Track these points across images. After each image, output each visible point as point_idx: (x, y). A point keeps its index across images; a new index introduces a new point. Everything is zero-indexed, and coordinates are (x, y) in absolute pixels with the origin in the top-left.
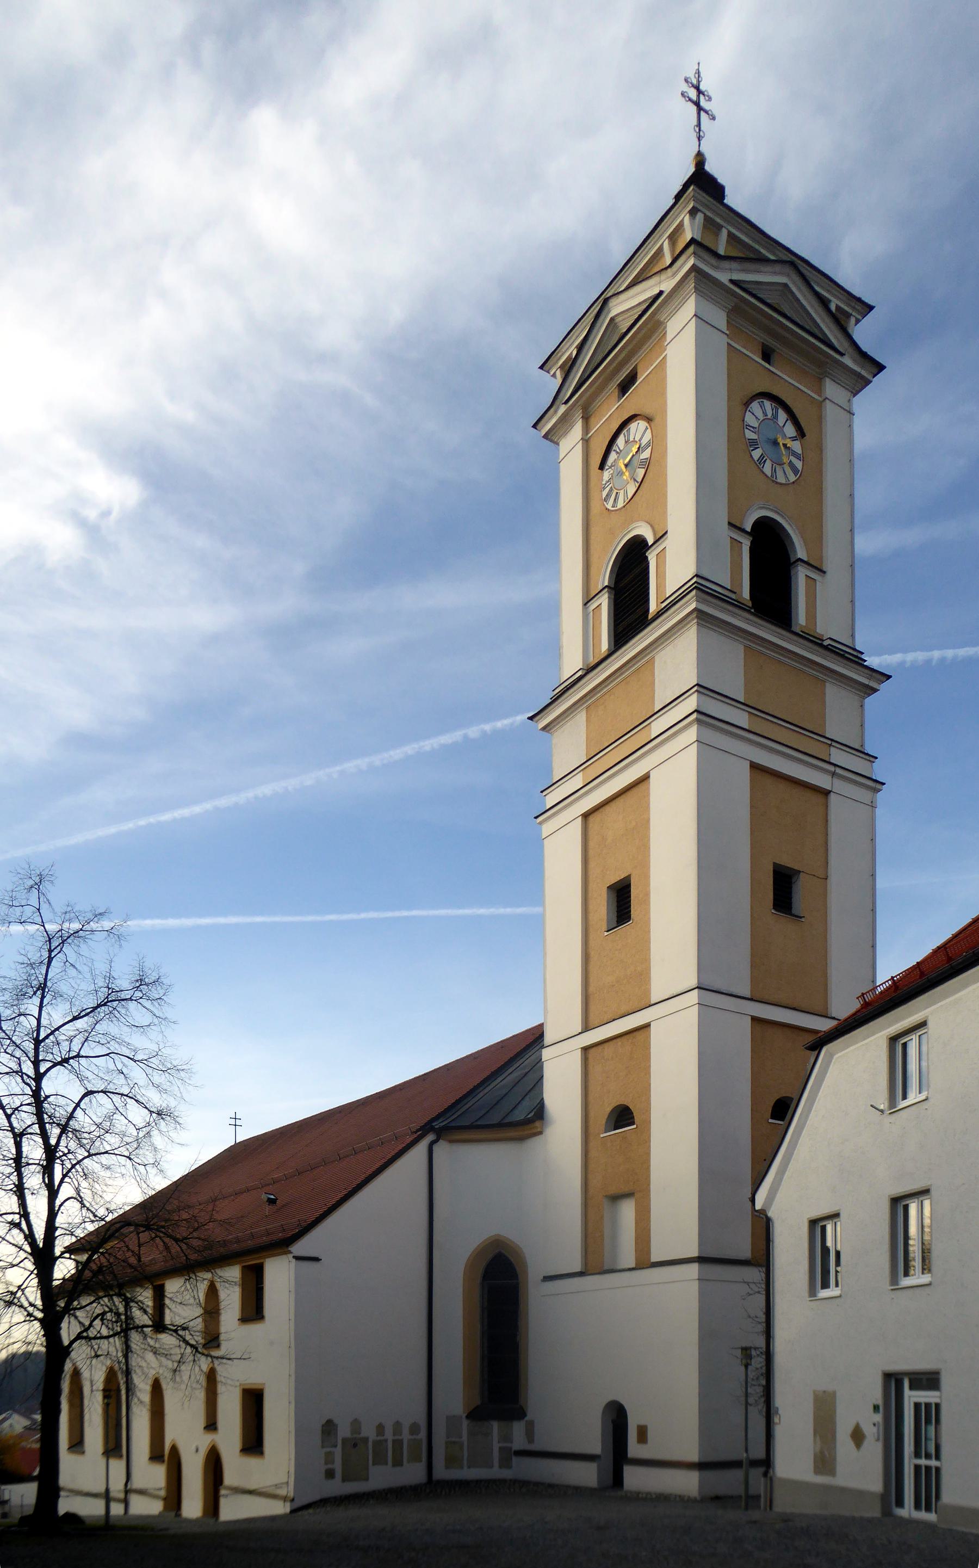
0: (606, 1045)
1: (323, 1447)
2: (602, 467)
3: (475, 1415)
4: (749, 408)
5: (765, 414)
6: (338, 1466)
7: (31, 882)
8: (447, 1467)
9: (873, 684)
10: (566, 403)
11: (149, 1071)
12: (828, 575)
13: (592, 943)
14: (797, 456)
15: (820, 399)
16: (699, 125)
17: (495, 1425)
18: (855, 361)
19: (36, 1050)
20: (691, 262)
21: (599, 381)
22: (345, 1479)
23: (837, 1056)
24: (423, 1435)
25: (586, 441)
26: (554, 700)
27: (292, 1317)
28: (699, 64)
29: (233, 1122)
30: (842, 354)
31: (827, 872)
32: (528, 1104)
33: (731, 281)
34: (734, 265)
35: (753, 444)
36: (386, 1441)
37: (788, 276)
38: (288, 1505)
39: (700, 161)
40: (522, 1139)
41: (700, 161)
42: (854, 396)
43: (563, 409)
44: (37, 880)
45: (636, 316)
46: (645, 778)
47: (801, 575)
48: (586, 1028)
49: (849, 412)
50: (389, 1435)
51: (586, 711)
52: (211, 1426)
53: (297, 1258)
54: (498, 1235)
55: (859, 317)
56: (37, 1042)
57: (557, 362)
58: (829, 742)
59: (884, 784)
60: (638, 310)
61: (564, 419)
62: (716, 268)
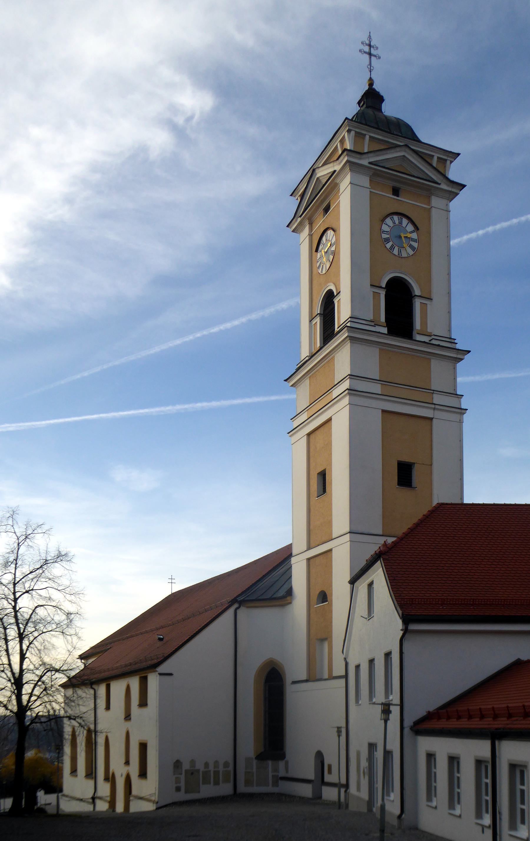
0: (317, 558)
1: (174, 774)
2: (317, 251)
3: (261, 757)
4: (384, 222)
5: (394, 223)
6: (182, 784)
7: (8, 515)
8: (246, 786)
9: (460, 356)
10: (300, 216)
11: (65, 594)
12: (434, 300)
13: (312, 503)
14: (415, 241)
15: (429, 207)
16: (370, 64)
17: (270, 763)
18: (448, 186)
19: (14, 587)
20: (346, 159)
21: (314, 208)
22: (186, 792)
23: (359, 588)
24: (231, 768)
25: (311, 235)
26: (298, 370)
27: (158, 706)
28: (370, 33)
29: (170, 581)
30: (440, 184)
31: (432, 462)
32: (286, 588)
33: (370, 163)
34: (372, 155)
35: (387, 240)
36: (210, 771)
37: (405, 151)
38: (155, 805)
39: (371, 83)
40: (283, 606)
41: (371, 83)
42: (450, 202)
43: (299, 219)
44: (12, 513)
45: (327, 178)
46: (330, 420)
47: (417, 304)
48: (309, 548)
49: (447, 211)
50: (211, 768)
51: (310, 379)
52: (127, 763)
53: (160, 674)
54: (271, 658)
55: (452, 160)
56: (15, 584)
57: (298, 193)
58: (432, 392)
59: (467, 410)
60: (328, 175)
61: (301, 224)
62: (360, 159)
